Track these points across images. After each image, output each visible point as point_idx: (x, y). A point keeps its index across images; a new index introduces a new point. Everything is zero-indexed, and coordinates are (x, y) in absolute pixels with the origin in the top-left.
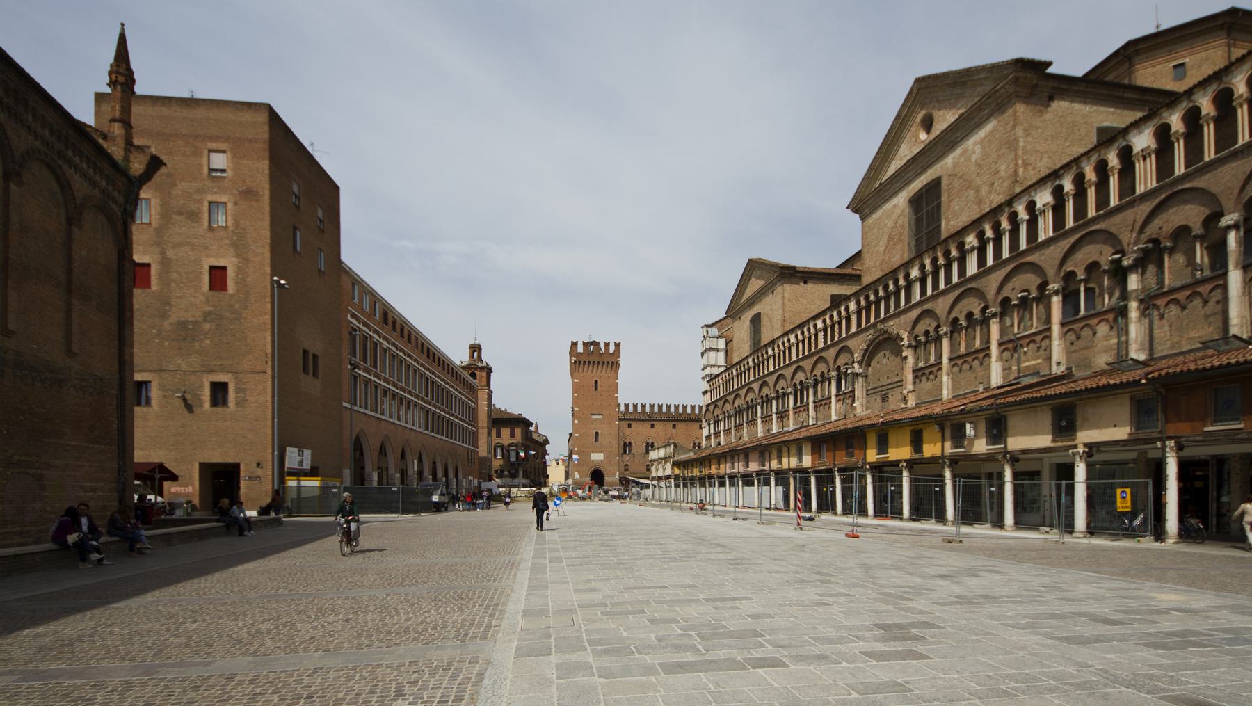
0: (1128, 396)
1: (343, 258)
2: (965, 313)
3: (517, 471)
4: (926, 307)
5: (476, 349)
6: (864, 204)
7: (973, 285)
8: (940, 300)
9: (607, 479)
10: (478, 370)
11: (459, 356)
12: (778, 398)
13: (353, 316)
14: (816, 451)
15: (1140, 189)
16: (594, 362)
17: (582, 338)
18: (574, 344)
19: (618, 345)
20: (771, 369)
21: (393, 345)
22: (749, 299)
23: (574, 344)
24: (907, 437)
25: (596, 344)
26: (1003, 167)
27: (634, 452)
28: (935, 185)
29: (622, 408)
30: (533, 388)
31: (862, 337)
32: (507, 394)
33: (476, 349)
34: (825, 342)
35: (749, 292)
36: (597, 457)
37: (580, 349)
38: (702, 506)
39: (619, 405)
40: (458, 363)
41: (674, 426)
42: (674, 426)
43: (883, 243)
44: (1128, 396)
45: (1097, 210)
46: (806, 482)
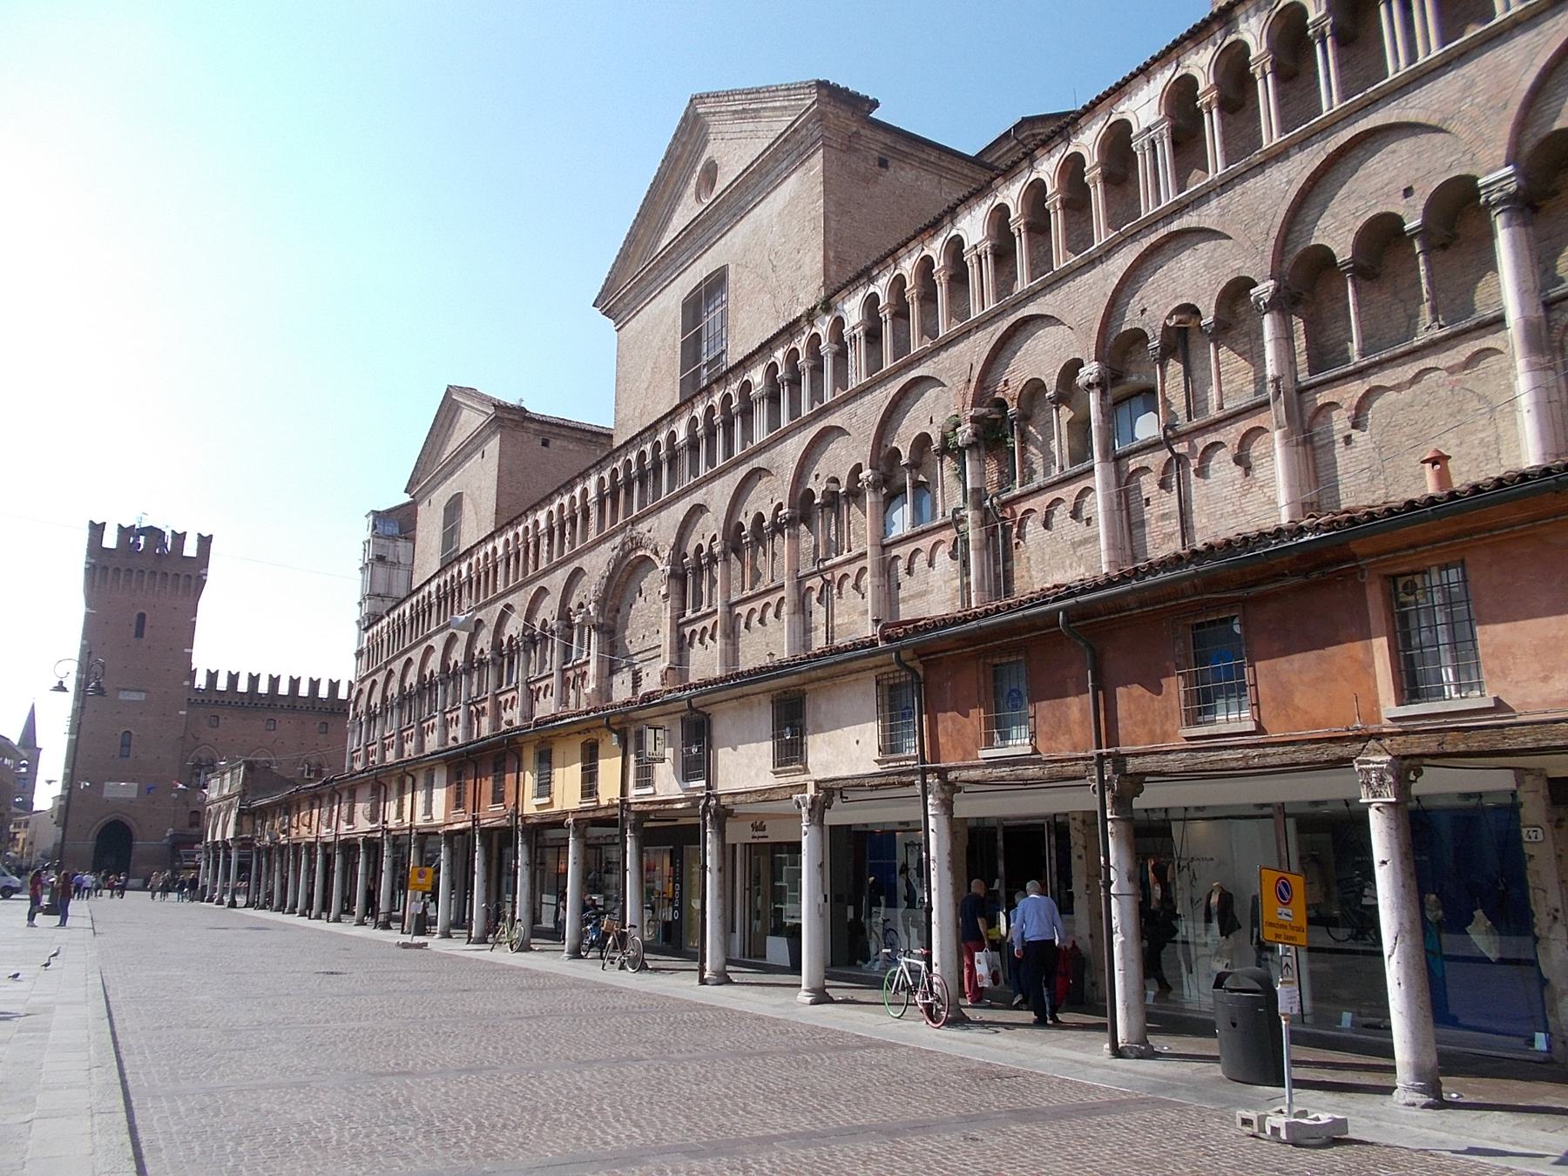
0: (872, 674)
2: (751, 516)
4: (576, 564)
6: (617, 300)
7: (1031, 309)
8: (717, 484)
12: (1284, 303)
15: (976, 313)
17: (119, 514)
19: (205, 542)
20: (500, 589)
22: (688, 231)
23: (97, 530)
24: (764, 717)
25: (154, 533)
26: (807, 260)
28: (716, 283)
29: (201, 681)
31: (608, 545)
34: (550, 559)
36: (122, 790)
38: (1094, 984)
39: (192, 675)
43: (646, 375)
44: (872, 674)
45: (1284, 129)
46: (328, 861)
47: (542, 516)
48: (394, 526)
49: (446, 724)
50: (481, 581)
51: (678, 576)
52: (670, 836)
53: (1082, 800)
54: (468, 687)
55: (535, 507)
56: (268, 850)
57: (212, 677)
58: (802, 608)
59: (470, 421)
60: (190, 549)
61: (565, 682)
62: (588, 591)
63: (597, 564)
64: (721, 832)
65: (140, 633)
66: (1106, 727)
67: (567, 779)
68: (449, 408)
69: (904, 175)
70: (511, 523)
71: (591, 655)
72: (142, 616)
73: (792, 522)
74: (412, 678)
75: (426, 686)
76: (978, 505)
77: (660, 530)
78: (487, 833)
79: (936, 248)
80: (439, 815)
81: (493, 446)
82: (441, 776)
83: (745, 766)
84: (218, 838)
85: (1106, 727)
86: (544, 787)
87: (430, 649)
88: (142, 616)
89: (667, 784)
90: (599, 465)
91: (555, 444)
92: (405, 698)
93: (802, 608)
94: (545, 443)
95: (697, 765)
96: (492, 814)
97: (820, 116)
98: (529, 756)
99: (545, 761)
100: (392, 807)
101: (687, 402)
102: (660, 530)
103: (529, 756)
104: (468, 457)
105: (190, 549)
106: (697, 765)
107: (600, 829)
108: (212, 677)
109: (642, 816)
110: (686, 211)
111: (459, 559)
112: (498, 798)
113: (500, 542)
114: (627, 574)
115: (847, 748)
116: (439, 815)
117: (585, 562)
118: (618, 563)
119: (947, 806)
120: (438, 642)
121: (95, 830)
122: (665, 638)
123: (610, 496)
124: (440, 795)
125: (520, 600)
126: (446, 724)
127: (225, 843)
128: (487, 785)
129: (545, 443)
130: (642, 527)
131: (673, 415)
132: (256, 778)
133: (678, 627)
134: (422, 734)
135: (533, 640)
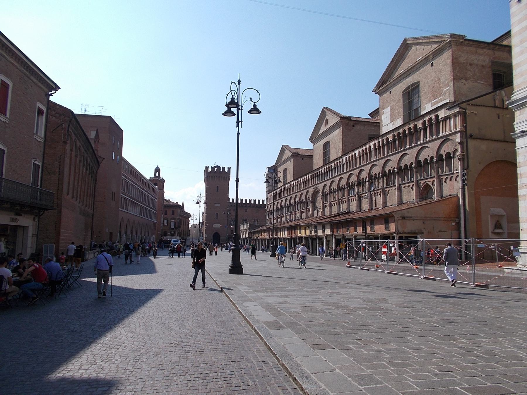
1: (123, 156)
3: (175, 232)
5: (157, 170)
9: (222, 238)
10: (158, 181)
11: (148, 174)
13: (124, 175)
14: (332, 228)
16: (217, 179)
17: (211, 165)
18: (207, 168)
19: (229, 169)
21: (133, 182)
23: (207, 168)
25: (218, 167)
27: (232, 225)
28: (328, 143)
29: (231, 201)
30: (187, 193)
31: (312, 188)
32: (171, 194)
33: (157, 170)
35: (401, 70)
36: (216, 226)
37: (210, 169)
40: (148, 178)
41: (258, 211)
42: (258, 211)
47: (302, 179)
48: (273, 170)
49: (286, 216)
50: (291, 188)
51: (323, 195)
52: (313, 239)
53: (341, 237)
54: (290, 209)
55: (301, 177)
56: (255, 240)
57: (242, 200)
58: (339, 205)
59: (288, 154)
60: (226, 170)
61: (307, 211)
62: (310, 195)
63: (311, 190)
64: (326, 239)
65: (218, 191)
66: (343, 232)
67: (303, 231)
68: (284, 149)
69: (357, 127)
70: (297, 179)
71: (310, 206)
72: (218, 187)
73: (338, 191)
74: (279, 206)
75: (282, 208)
76: (358, 194)
77: (320, 186)
78: (293, 238)
79: (353, 154)
80: (286, 236)
81: (292, 160)
82: (286, 229)
83: (320, 232)
84: (244, 237)
85: (343, 232)
86: (300, 233)
87: (282, 201)
88: (218, 187)
89: (313, 234)
90: (311, 173)
91: (304, 159)
92: (278, 209)
93: (339, 205)
94: (302, 159)
95: (316, 232)
96: (294, 236)
97: (341, 121)
98: (298, 228)
99: (300, 229)
100: (279, 234)
101: (324, 166)
102: (320, 186)
103: (298, 228)
104: (287, 161)
105: (226, 170)
106: (316, 232)
107: (307, 238)
108: (242, 200)
109: (311, 237)
110: (323, 129)
111: (287, 184)
112: (295, 234)
113: (294, 182)
114: (316, 193)
115: (328, 232)
116: (286, 236)
117: (309, 190)
118: (314, 191)
119: (335, 238)
120: (284, 199)
121: (212, 235)
122: (321, 205)
123: (313, 178)
124: (286, 232)
125: (299, 194)
126: (286, 216)
127: (246, 238)
128: (293, 232)
129: (302, 159)
130: (318, 186)
131: (322, 167)
132: (251, 227)
133: (323, 204)
134: (281, 217)
135: (301, 202)
